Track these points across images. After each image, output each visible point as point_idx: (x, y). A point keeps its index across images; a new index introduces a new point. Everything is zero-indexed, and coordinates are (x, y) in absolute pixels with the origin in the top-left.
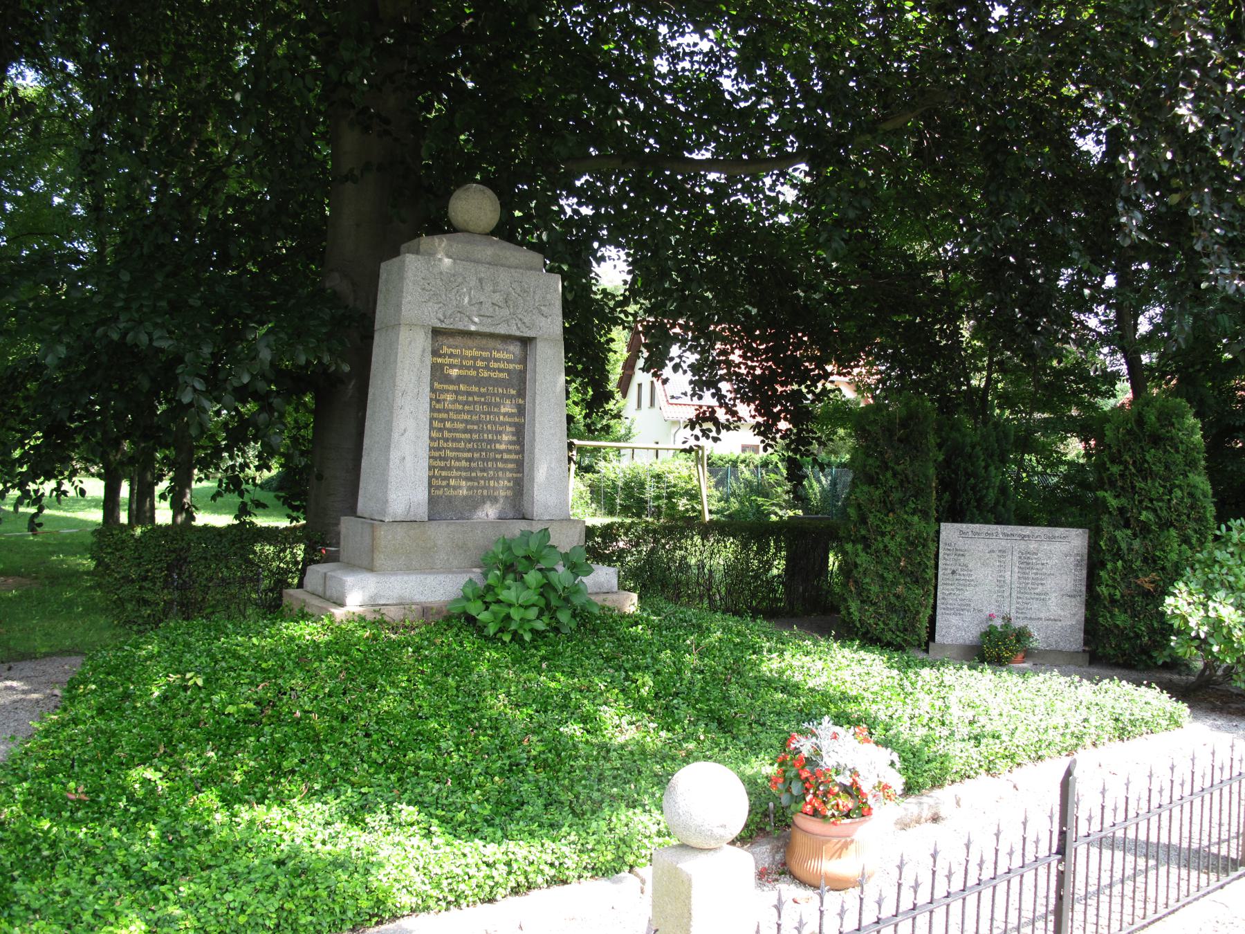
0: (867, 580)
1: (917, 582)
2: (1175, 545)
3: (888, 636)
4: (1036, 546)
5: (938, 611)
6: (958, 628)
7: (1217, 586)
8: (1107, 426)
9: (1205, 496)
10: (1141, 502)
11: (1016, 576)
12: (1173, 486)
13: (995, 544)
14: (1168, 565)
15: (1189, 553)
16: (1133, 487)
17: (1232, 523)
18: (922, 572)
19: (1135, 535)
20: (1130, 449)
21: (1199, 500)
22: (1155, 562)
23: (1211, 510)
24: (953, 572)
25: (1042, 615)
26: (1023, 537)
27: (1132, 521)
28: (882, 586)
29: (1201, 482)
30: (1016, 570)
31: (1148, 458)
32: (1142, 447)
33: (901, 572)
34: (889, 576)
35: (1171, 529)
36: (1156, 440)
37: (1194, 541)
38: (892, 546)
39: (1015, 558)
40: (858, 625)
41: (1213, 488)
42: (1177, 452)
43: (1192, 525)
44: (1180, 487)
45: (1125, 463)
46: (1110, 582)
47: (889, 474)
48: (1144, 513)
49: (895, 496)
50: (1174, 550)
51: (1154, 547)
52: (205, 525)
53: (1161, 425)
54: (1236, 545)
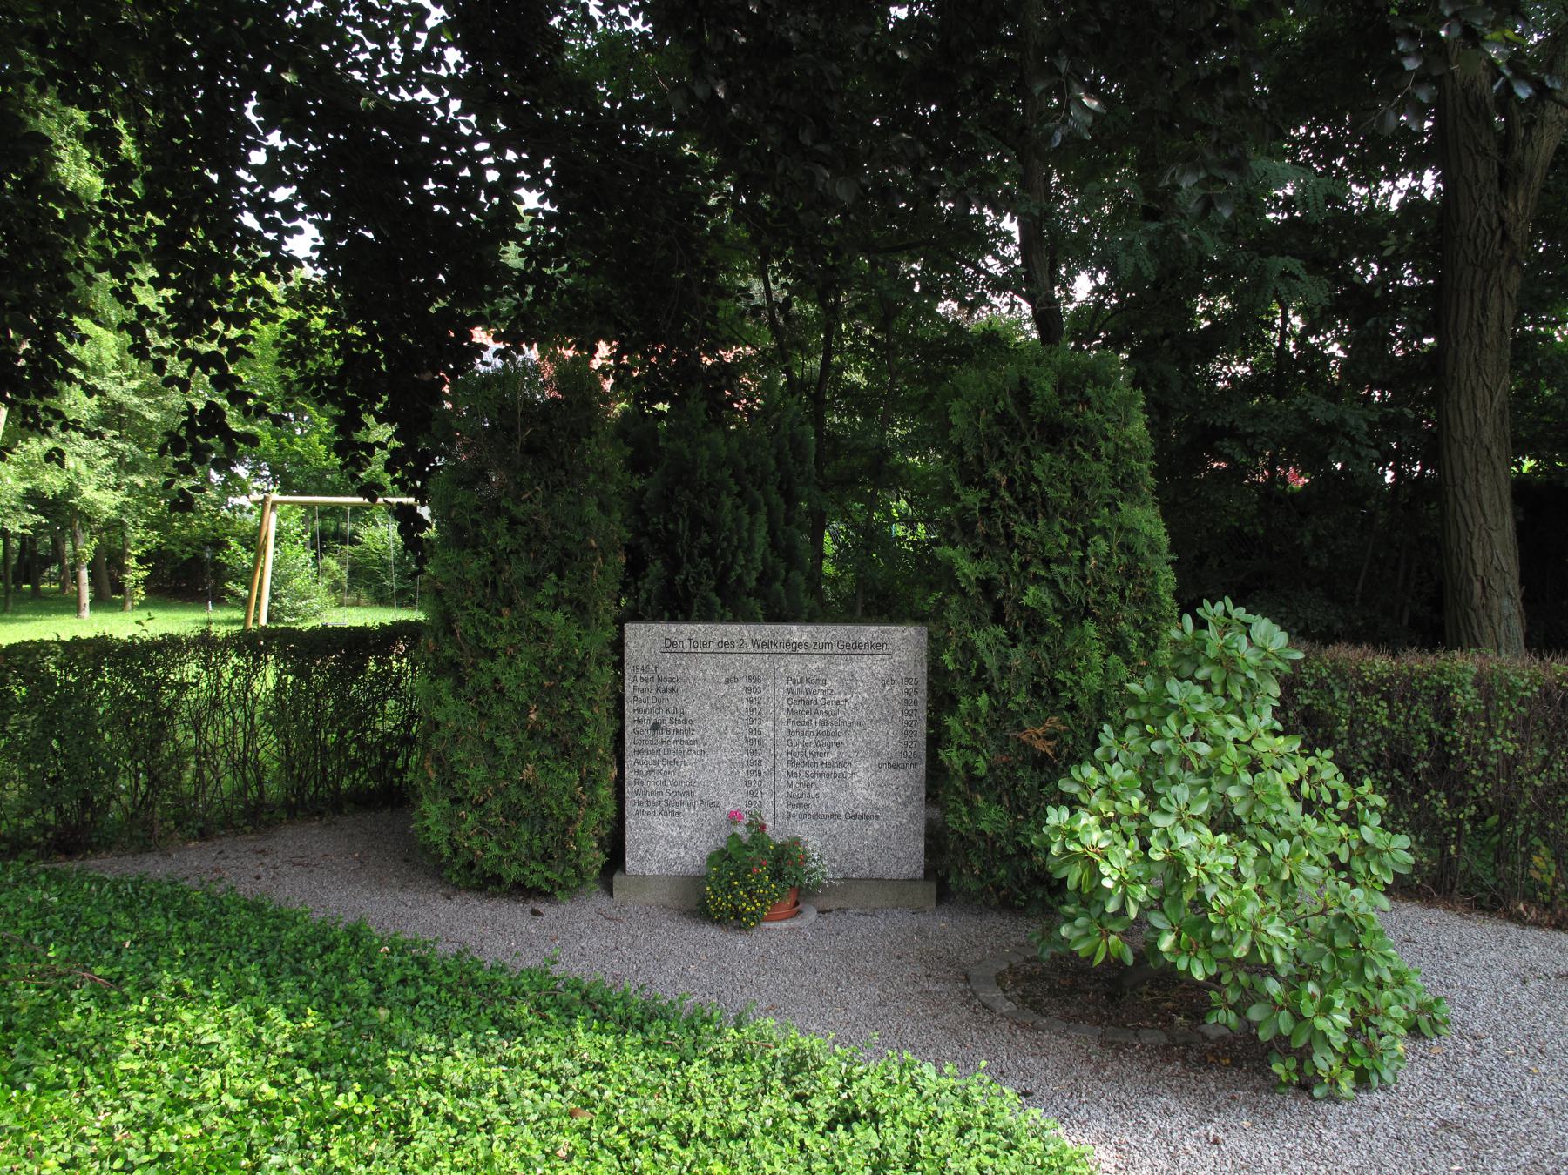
0: (461, 755)
1: (566, 753)
2: (1096, 657)
3: (512, 872)
4: (821, 665)
5: (630, 809)
6: (671, 842)
7: (1172, 768)
8: (956, 405)
9: (1154, 550)
10: (1024, 566)
11: (783, 730)
12: (1090, 531)
13: (739, 664)
14: (1082, 700)
15: (1124, 672)
16: (1009, 536)
17: (1208, 610)
18: (585, 736)
19: (1014, 639)
20: (1002, 454)
21: (1143, 559)
22: (1055, 693)
23: (1167, 580)
24: (656, 727)
25: (841, 809)
26: (795, 648)
27: (1008, 608)
28: (492, 767)
29: (1147, 521)
30: (783, 716)
31: (1037, 471)
32: (1026, 450)
33: (532, 735)
34: (507, 745)
35: (1087, 622)
36: (1054, 434)
37: (1133, 646)
38: (508, 680)
40: (447, 852)
41: (1170, 533)
42: (1097, 457)
43: (1130, 611)
44: (1103, 532)
45: (990, 485)
46: (966, 739)
47: (502, 523)
48: (1031, 590)
49: (516, 571)
50: (1093, 667)
51: (1054, 662)
52: (104, 637)
53: (1064, 403)
54: (1217, 662)
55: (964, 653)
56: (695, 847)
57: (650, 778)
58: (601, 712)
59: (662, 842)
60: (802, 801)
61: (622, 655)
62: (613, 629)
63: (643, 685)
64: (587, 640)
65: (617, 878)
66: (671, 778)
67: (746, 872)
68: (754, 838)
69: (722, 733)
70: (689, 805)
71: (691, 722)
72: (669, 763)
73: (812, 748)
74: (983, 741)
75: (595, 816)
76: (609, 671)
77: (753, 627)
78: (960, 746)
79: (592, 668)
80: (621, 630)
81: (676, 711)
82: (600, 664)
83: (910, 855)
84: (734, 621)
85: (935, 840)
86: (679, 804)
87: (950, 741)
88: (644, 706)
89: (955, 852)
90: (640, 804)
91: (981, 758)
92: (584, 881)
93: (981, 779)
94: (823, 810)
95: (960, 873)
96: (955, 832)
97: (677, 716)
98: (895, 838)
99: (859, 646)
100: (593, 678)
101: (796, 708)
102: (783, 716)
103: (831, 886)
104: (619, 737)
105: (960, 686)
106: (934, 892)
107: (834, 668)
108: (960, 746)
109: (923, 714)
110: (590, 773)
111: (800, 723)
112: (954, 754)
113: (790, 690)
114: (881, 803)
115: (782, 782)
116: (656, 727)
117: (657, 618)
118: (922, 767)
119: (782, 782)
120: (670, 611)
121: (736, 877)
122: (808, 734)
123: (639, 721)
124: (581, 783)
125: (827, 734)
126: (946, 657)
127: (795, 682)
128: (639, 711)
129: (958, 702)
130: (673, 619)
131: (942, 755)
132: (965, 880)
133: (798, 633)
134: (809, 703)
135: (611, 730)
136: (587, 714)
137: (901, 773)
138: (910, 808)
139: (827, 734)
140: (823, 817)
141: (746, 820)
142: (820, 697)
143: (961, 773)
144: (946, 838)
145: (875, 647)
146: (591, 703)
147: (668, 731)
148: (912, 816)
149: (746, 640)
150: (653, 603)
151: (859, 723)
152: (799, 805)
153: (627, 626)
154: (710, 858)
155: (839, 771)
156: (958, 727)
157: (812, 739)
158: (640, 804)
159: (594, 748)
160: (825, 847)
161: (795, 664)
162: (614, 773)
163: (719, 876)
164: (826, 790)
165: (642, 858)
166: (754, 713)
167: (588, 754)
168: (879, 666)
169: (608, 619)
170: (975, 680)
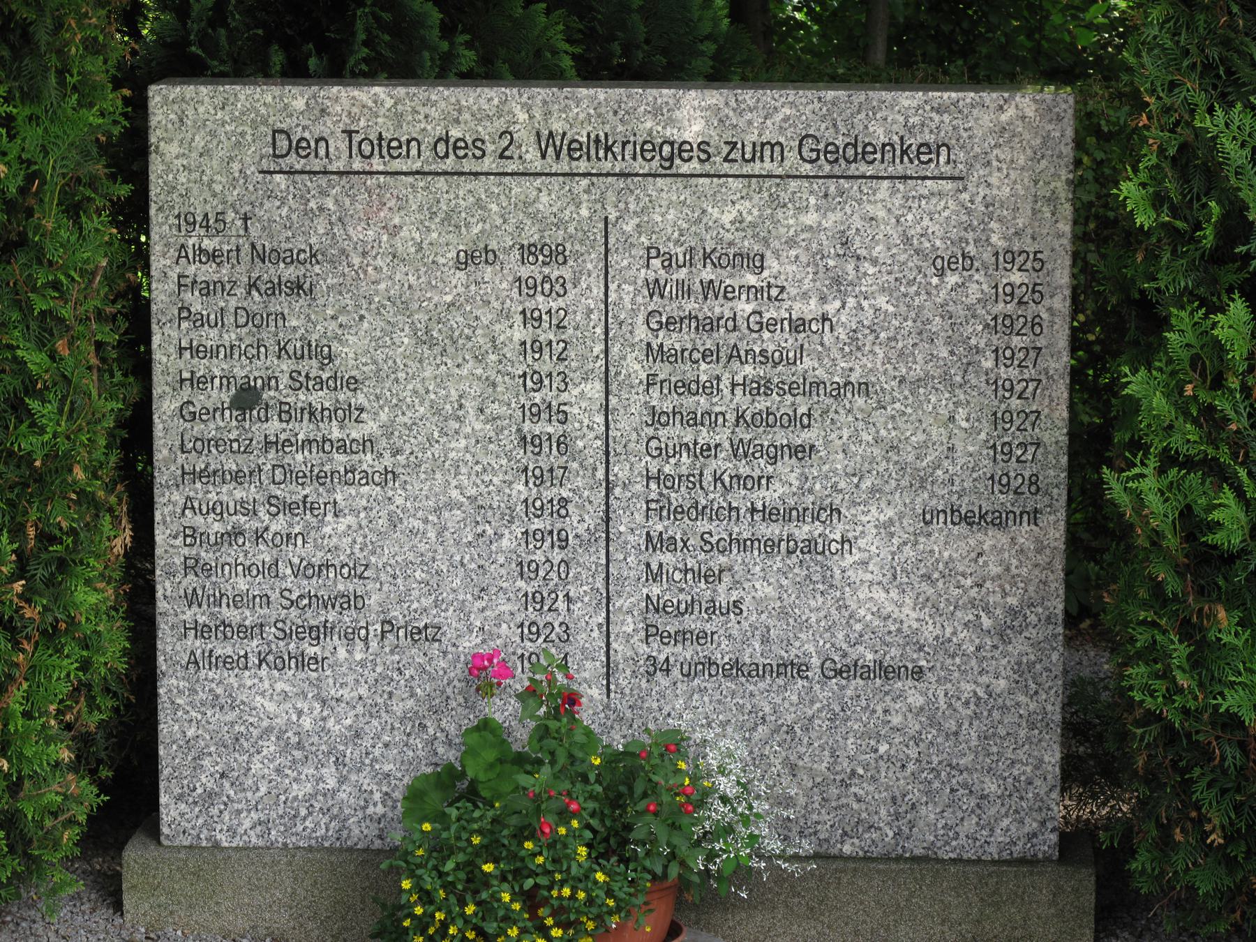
4: (749, 209)
6: (296, 747)
13: (504, 209)
24: (247, 399)
25: (809, 648)
26: (670, 157)
30: (634, 367)
39: (625, 295)
46: (1188, 438)
55: (1184, 178)
56: (367, 761)
57: (230, 554)
58: (78, 355)
59: (270, 747)
60: (692, 623)
61: (140, 180)
62: (113, 100)
63: (207, 272)
64: (31, 136)
65: (135, 855)
66: (295, 553)
67: (521, 835)
68: (543, 733)
69: (449, 417)
70: (349, 637)
71: (354, 384)
72: (288, 508)
73: (722, 463)
74: (1238, 445)
75: (63, 670)
76: (99, 225)
77: (541, 93)
78: (1169, 460)
79: (50, 219)
80: (138, 108)
81: (310, 350)
82: (74, 209)
83: (1017, 788)
84: (484, 72)
85: (1094, 741)
86: (319, 633)
87: (1137, 445)
88: (210, 337)
89: (1151, 778)
90: (201, 631)
91: (1228, 497)
92: (33, 865)
93: (1229, 559)
94: (753, 652)
95: (1165, 843)
96: (1152, 717)
97: (311, 366)
98: (972, 735)
99: (862, 151)
100: (54, 253)
101: (671, 341)
102: (634, 367)
103: (780, 877)
104: (136, 431)
105: (1171, 277)
106: (1089, 900)
107: (789, 221)
108: (1169, 460)
109: (1059, 362)
110: (47, 538)
111: (684, 388)
112: (1149, 484)
113: (655, 288)
114: (929, 632)
115: (629, 565)
116: (247, 399)
117: (246, 66)
118: (1054, 530)
119: (629, 565)
120: (288, 45)
121: (490, 851)
122: (711, 419)
123: (197, 382)
124: (22, 570)
125: (767, 419)
126: (1129, 190)
127: (669, 262)
128: (195, 351)
129: (1164, 323)
130: (296, 72)
131: (1115, 486)
132: (1179, 861)
133: (692, 113)
134: (711, 325)
135: (110, 408)
136: (35, 360)
137: (991, 539)
138: (1019, 646)
139: (767, 419)
140: (757, 671)
141: (520, 683)
142: (745, 307)
143: (1172, 542)
144: (1124, 736)
145: (917, 157)
146: (47, 329)
147: (286, 413)
148: (1021, 669)
149: (523, 134)
150: (236, 20)
151: (864, 388)
152: (681, 636)
153: (164, 101)
154: (415, 796)
155: (803, 531)
156: (1159, 402)
157: (722, 436)
158: (201, 631)
159: (59, 462)
160: (759, 760)
161: (667, 209)
162: (123, 539)
163: (440, 849)
164: (765, 590)
165: (210, 796)
166: (545, 355)
167: (41, 480)
168: (935, 214)
169: (97, 69)
170: (1220, 256)
